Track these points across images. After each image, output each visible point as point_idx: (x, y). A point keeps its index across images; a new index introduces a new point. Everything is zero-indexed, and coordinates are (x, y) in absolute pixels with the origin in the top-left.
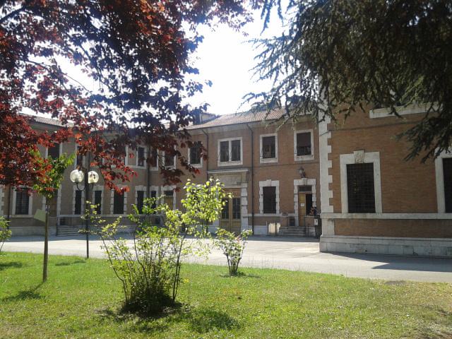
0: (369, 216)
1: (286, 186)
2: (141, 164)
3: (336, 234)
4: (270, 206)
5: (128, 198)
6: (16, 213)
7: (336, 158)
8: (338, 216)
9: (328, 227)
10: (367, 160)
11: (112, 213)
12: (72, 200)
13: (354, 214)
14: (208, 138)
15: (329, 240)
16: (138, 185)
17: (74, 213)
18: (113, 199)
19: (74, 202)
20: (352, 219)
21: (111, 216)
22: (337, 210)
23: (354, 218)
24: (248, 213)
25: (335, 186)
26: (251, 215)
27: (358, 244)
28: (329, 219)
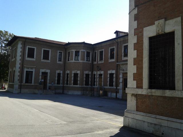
0: (168, 93)
1: (82, 74)
2: (76, 59)
3: (137, 110)
4: (28, 80)
5: (80, 77)
6: (25, 83)
7: (141, 32)
8: (140, 92)
9: (131, 102)
10: (168, 29)
11: (72, 84)
12: (56, 77)
13: (153, 90)
14: (118, 44)
15: (130, 115)
16: (58, 70)
17: (56, 84)
18: (73, 78)
19: (56, 79)
20: (152, 96)
21: (72, 86)
22: (139, 86)
23: (154, 94)
24: (19, 83)
25: (138, 62)
26: (20, 84)
27: (155, 125)
28: (133, 95)
